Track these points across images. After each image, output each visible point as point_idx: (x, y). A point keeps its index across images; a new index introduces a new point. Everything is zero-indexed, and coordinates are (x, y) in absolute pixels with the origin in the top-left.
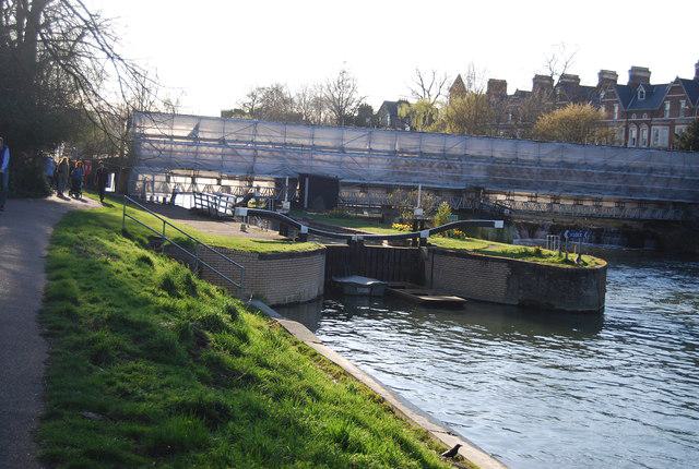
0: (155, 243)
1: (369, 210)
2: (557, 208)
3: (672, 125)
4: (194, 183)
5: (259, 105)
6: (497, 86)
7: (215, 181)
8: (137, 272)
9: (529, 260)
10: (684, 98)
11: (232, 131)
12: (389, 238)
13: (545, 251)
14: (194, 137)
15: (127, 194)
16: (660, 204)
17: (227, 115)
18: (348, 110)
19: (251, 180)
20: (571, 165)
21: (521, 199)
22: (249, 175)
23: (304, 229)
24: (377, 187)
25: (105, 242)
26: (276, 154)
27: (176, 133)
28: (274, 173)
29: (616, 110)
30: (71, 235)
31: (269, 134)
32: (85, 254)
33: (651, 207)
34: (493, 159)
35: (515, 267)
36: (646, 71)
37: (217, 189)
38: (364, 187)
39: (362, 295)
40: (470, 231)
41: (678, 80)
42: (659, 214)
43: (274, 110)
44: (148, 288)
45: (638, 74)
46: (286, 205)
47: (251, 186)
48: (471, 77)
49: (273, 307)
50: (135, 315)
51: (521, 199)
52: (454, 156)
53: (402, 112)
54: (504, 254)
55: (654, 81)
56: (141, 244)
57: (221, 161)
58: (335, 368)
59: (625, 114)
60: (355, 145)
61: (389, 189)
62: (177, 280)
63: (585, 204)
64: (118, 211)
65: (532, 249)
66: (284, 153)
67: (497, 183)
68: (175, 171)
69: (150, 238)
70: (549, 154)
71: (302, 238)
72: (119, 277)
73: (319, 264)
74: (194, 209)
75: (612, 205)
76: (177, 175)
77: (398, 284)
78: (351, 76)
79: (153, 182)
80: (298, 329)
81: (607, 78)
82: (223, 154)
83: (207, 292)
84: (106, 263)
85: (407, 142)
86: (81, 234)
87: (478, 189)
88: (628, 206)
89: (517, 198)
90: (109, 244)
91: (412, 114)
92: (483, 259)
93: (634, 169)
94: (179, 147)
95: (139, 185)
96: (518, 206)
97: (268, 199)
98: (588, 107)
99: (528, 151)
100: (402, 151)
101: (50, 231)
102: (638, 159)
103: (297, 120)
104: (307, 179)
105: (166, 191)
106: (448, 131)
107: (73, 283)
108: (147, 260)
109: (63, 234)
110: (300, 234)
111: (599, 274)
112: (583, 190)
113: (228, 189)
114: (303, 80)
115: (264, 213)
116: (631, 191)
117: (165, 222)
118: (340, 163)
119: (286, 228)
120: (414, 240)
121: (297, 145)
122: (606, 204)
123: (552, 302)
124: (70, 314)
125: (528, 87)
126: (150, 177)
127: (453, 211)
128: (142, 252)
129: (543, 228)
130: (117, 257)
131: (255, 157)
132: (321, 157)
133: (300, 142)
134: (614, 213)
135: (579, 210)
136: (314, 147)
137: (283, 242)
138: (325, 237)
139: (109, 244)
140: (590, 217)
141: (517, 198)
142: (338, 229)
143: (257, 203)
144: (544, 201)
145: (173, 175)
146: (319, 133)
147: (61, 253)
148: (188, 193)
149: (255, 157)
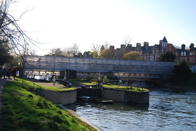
0: (31, 89)
1: (84, 78)
2: (130, 76)
3: (154, 56)
4: (39, 73)
5: (54, 53)
6: (112, 47)
7: (45, 72)
8: (29, 100)
9: (130, 90)
10: (157, 49)
11: (49, 60)
12: (92, 86)
13: (133, 88)
14: (39, 61)
15: (22, 76)
16: (155, 75)
17: (47, 56)
18: (76, 54)
19: (54, 72)
20: (133, 66)
21: (121, 74)
22: (53, 71)
23: (70, 84)
24: (85, 72)
25: (18, 90)
26: (60, 65)
27: (35, 60)
28: (60, 70)
29: (141, 52)
30: (8, 89)
31: (58, 60)
32: (12, 95)
33: (153, 75)
34: (114, 65)
35: (126, 92)
36: (148, 43)
37: (45, 74)
38: (82, 73)
39: (87, 101)
40: (111, 83)
41: (155, 45)
42: (155, 77)
43: (58, 54)
44: (34, 106)
45: (146, 44)
46: (65, 78)
47: (54, 73)
48: (106, 45)
49: (64, 106)
50: (33, 119)
51: (121, 74)
52: (104, 64)
53: (90, 54)
54: (123, 89)
55: (149, 45)
56: (28, 91)
57: (46, 67)
58: (86, 124)
59: (143, 53)
60: (80, 62)
61: (89, 73)
62: (42, 103)
63: (137, 75)
64: (20, 81)
65: (129, 87)
66: (62, 65)
67: (115, 71)
68: (34, 70)
69: (30, 88)
70: (128, 63)
71: (70, 87)
72: (24, 102)
73: (75, 94)
74: (40, 80)
75: (143, 75)
76: (35, 71)
77: (95, 97)
78: (77, 46)
79: (29, 73)
80: (71, 111)
81: (138, 45)
82: (47, 65)
83: (50, 105)
84: (20, 98)
85: (93, 61)
86: (11, 88)
87: (111, 72)
88: (147, 75)
89: (120, 74)
90: (20, 91)
91: (92, 54)
92: (118, 90)
93: (148, 66)
94: (36, 64)
95: (25, 74)
96: (121, 76)
97: (58, 76)
98: (135, 51)
99: (123, 63)
100: (92, 63)
101: (2, 88)
102: (149, 64)
103: (63, 56)
104: (68, 71)
105: (32, 75)
106: (101, 58)
107: (10, 106)
108: (31, 96)
109: (6, 89)
110: (69, 86)
111: (148, 93)
112: (136, 72)
113: (48, 74)
114: (65, 46)
115: (60, 80)
116: (148, 71)
117: (34, 84)
118: (76, 67)
119: (66, 84)
120: (99, 86)
121: (66, 63)
122: (142, 75)
123: (136, 101)
124: (10, 120)
125: (120, 47)
126: (28, 72)
127: (108, 78)
128: (30, 93)
129: (126, 81)
130: (22, 95)
131: (55, 66)
132: (71, 65)
133: (66, 62)
134: (144, 77)
135: (135, 77)
136: (70, 63)
137: (65, 88)
138: (75, 86)
139: (20, 91)
140: (139, 78)
141: (120, 74)
142: (78, 84)
143: (56, 77)
144: (127, 75)
145: (34, 71)
146: (71, 59)
147: (6, 95)
148: (38, 75)
149: (55, 66)
